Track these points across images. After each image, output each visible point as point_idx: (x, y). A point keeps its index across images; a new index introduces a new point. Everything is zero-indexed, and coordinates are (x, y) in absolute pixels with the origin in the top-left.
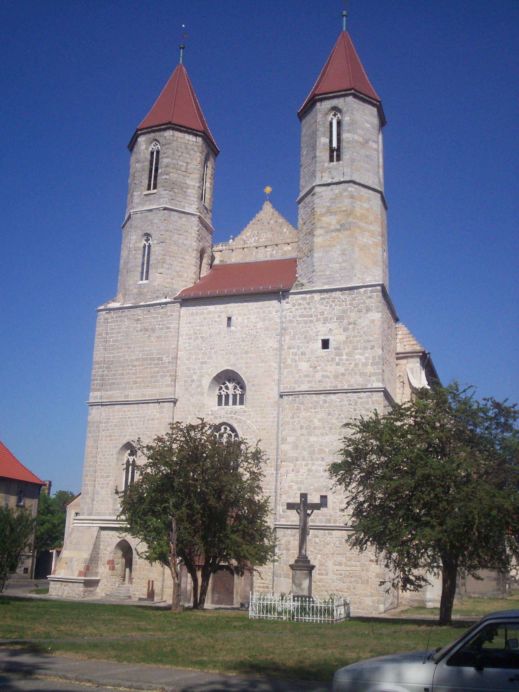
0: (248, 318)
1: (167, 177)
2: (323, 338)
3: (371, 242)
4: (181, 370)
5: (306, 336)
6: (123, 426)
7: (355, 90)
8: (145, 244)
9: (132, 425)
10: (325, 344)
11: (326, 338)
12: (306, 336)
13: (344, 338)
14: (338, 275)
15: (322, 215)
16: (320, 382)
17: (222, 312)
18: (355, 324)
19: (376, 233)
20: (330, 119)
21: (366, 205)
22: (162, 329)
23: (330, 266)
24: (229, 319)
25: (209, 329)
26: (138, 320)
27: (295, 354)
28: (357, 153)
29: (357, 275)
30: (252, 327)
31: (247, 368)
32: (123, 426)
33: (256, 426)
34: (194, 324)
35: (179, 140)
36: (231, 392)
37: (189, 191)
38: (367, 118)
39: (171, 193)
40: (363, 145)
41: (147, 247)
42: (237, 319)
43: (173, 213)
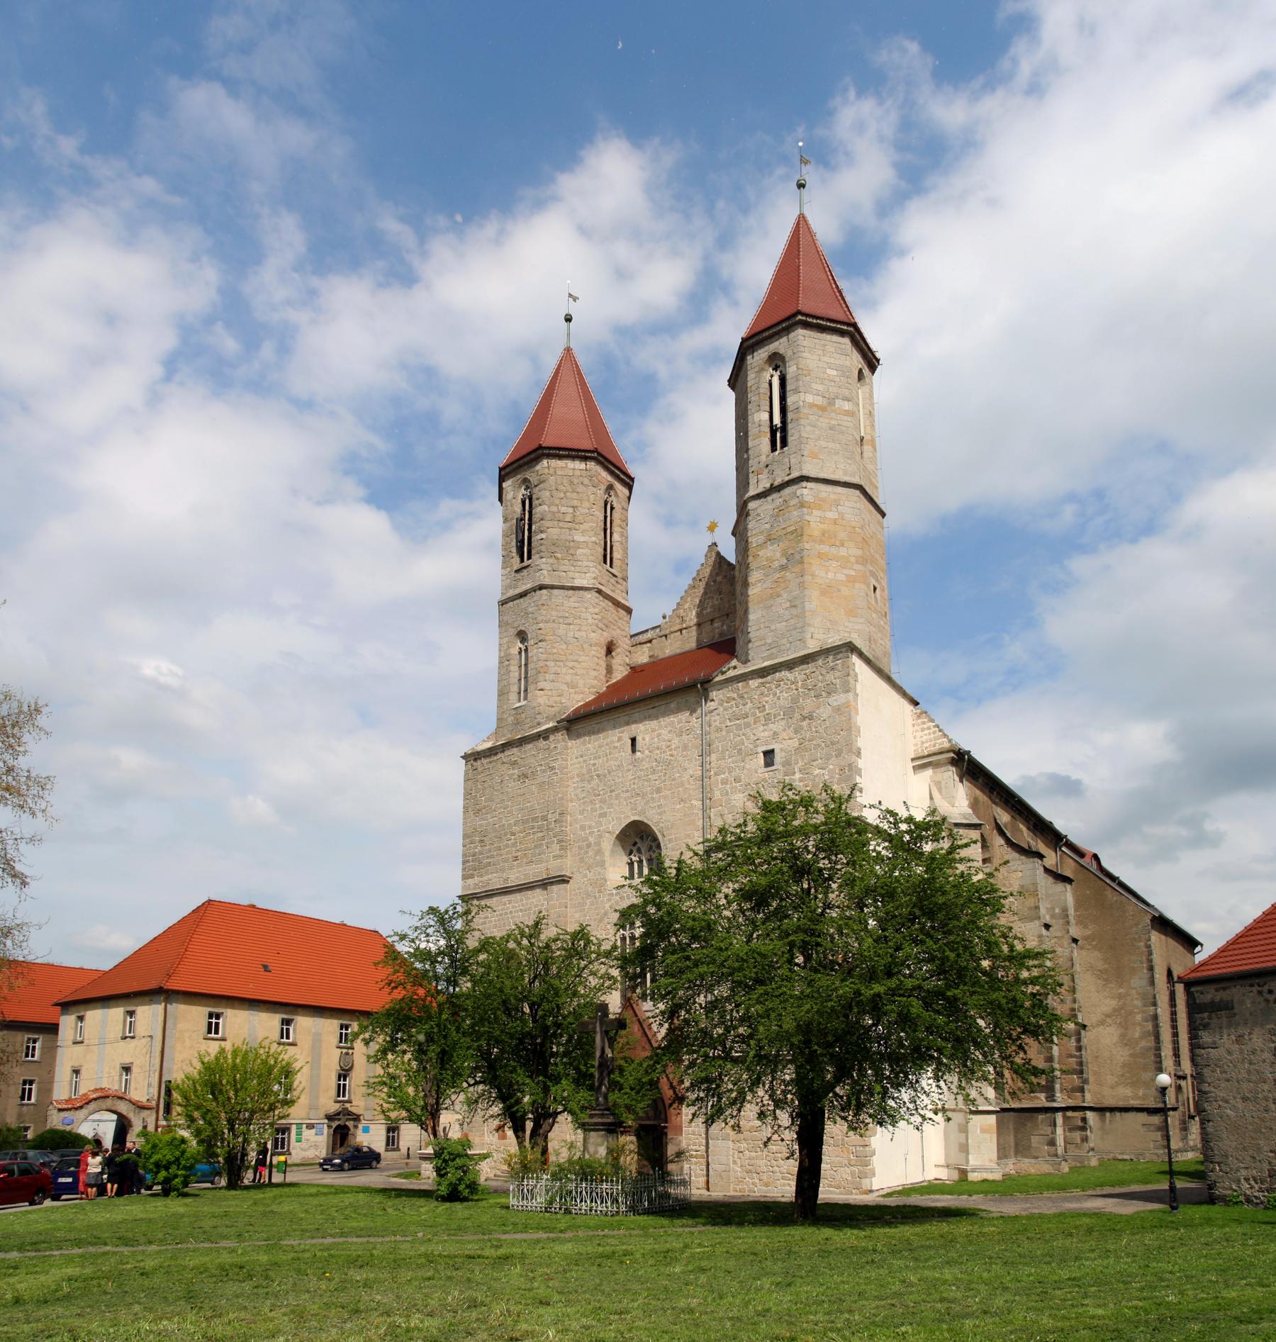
0: (659, 735)
1: (543, 536)
3: (842, 577)
7: (803, 314)
13: (796, 745)
14: (784, 641)
15: (761, 546)
18: (811, 718)
19: (853, 559)
21: (831, 515)
22: (544, 771)
23: (773, 627)
24: (633, 740)
26: (515, 763)
27: (724, 782)
29: (815, 636)
35: (559, 472)
37: (579, 551)
38: (832, 360)
39: (551, 561)
43: (556, 592)
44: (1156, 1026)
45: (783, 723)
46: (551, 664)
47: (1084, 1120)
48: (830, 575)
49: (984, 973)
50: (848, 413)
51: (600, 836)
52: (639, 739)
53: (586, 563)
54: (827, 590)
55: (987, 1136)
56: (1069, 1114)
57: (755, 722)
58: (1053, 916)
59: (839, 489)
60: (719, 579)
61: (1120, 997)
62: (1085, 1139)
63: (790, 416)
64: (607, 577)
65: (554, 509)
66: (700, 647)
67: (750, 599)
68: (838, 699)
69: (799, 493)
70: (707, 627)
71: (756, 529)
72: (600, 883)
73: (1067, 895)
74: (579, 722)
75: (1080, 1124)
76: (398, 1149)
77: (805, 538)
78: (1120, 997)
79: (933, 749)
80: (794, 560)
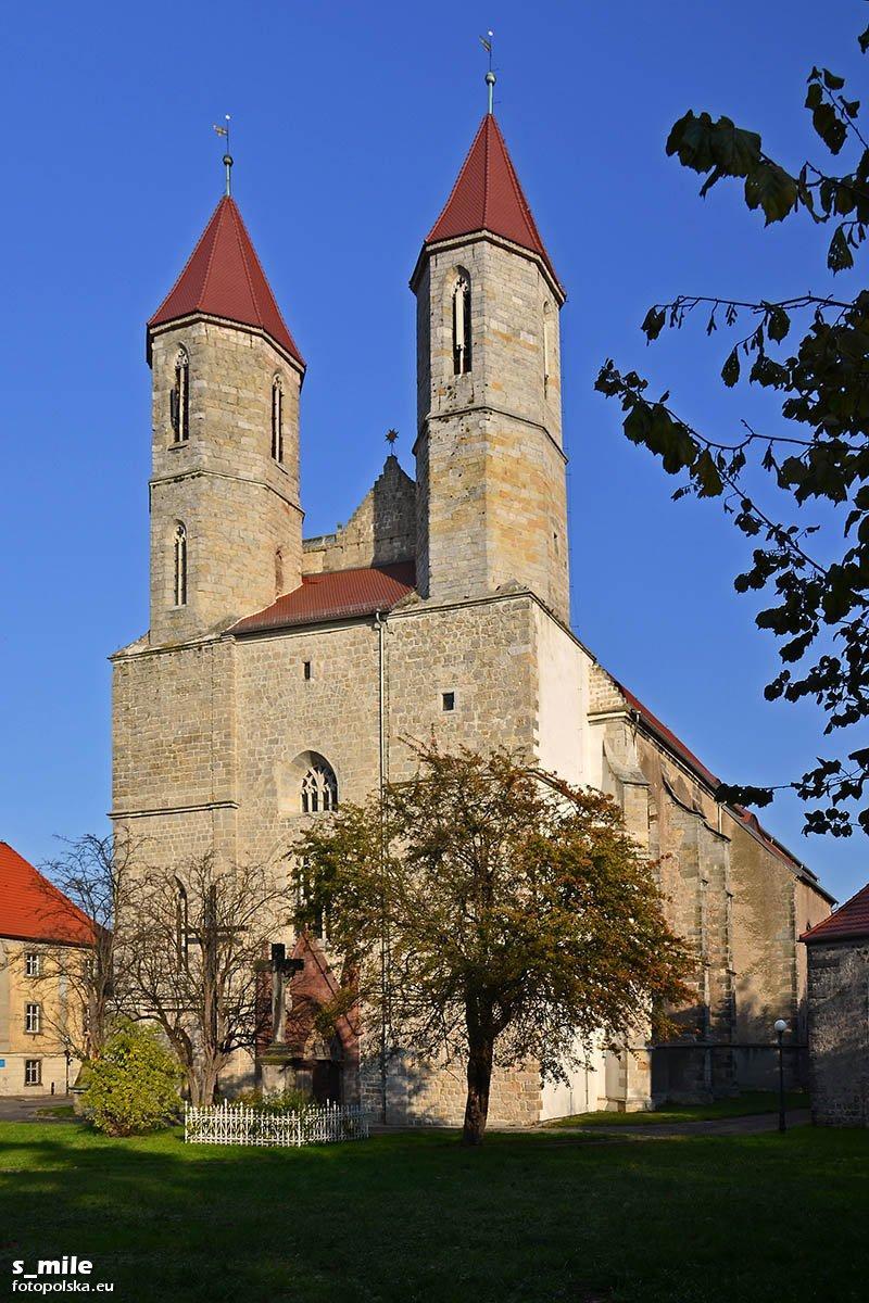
1: (202, 415)
4: (237, 753)
5: (420, 688)
9: (176, 848)
10: (449, 700)
11: (449, 691)
12: (420, 688)
14: (466, 581)
15: (443, 473)
19: (534, 504)
21: (515, 454)
24: (307, 664)
28: (496, 355)
30: (340, 677)
31: (336, 747)
40: (508, 339)
41: (180, 546)
42: (318, 665)
44: (795, 975)
45: (463, 667)
46: (212, 562)
47: (730, 1057)
48: (512, 517)
49: (592, 942)
50: (532, 348)
51: (271, 764)
53: (252, 455)
54: (508, 532)
55: (645, 1072)
56: (718, 1051)
58: (711, 872)
59: (523, 427)
60: (399, 495)
61: (766, 948)
62: (730, 1074)
63: (474, 338)
64: (275, 473)
65: (214, 386)
66: (376, 565)
68: (518, 649)
70: (386, 545)
71: (438, 452)
72: (271, 813)
73: (726, 853)
74: (248, 632)
75: (726, 1060)
76: (40, 1084)
77: (487, 473)
78: (766, 948)
79: (608, 707)
80: (476, 494)
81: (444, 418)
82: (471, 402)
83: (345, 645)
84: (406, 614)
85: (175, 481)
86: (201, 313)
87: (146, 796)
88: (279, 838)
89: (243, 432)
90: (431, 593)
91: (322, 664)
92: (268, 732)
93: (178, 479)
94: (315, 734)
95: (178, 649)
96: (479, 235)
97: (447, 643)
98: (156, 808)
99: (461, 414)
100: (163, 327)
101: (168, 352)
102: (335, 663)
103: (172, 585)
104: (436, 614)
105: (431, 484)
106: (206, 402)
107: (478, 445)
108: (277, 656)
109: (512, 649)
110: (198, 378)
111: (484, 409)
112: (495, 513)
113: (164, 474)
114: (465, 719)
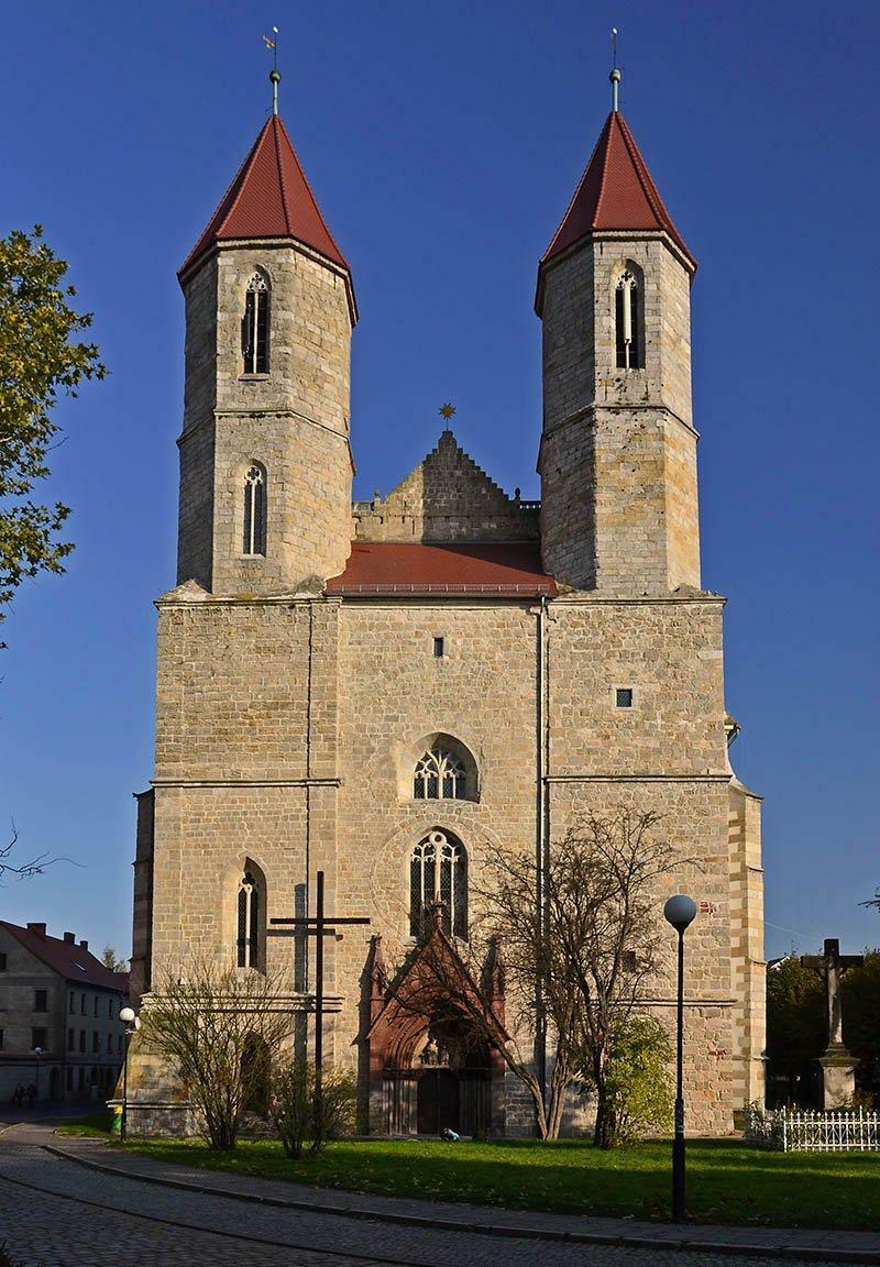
1: (289, 350)
2: (620, 686)
5: (589, 681)
6: (233, 827)
7: (349, 274)
8: (249, 482)
10: (625, 698)
11: (627, 687)
14: (642, 578)
16: (617, 762)
17: (424, 627)
18: (676, 666)
20: (617, 284)
24: (439, 641)
25: (399, 656)
27: (568, 712)
30: (483, 658)
32: (233, 827)
33: (499, 834)
34: (366, 646)
36: (442, 773)
51: (389, 742)
52: (448, 641)
57: (608, 657)
60: (458, 473)
65: (301, 322)
66: (428, 542)
67: (598, 518)
69: (659, 423)
70: (440, 524)
81: (615, 410)
82: (646, 399)
83: (491, 625)
84: (574, 602)
85: (251, 417)
86: (294, 238)
87: (207, 764)
88: (397, 824)
89: (325, 377)
90: (598, 585)
91: (459, 642)
92: (384, 707)
93: (257, 415)
94: (448, 716)
95: (260, 603)
96: (656, 234)
97: (624, 638)
98: (222, 779)
99: (634, 409)
100: (237, 243)
101: (239, 270)
102: (476, 643)
103: (240, 530)
104: (611, 607)
105: (598, 474)
106: (293, 338)
107: (655, 443)
108: (397, 626)
109: (702, 654)
110: (284, 309)
111: (663, 409)
112: (670, 515)
113: (233, 405)
114: (646, 717)
